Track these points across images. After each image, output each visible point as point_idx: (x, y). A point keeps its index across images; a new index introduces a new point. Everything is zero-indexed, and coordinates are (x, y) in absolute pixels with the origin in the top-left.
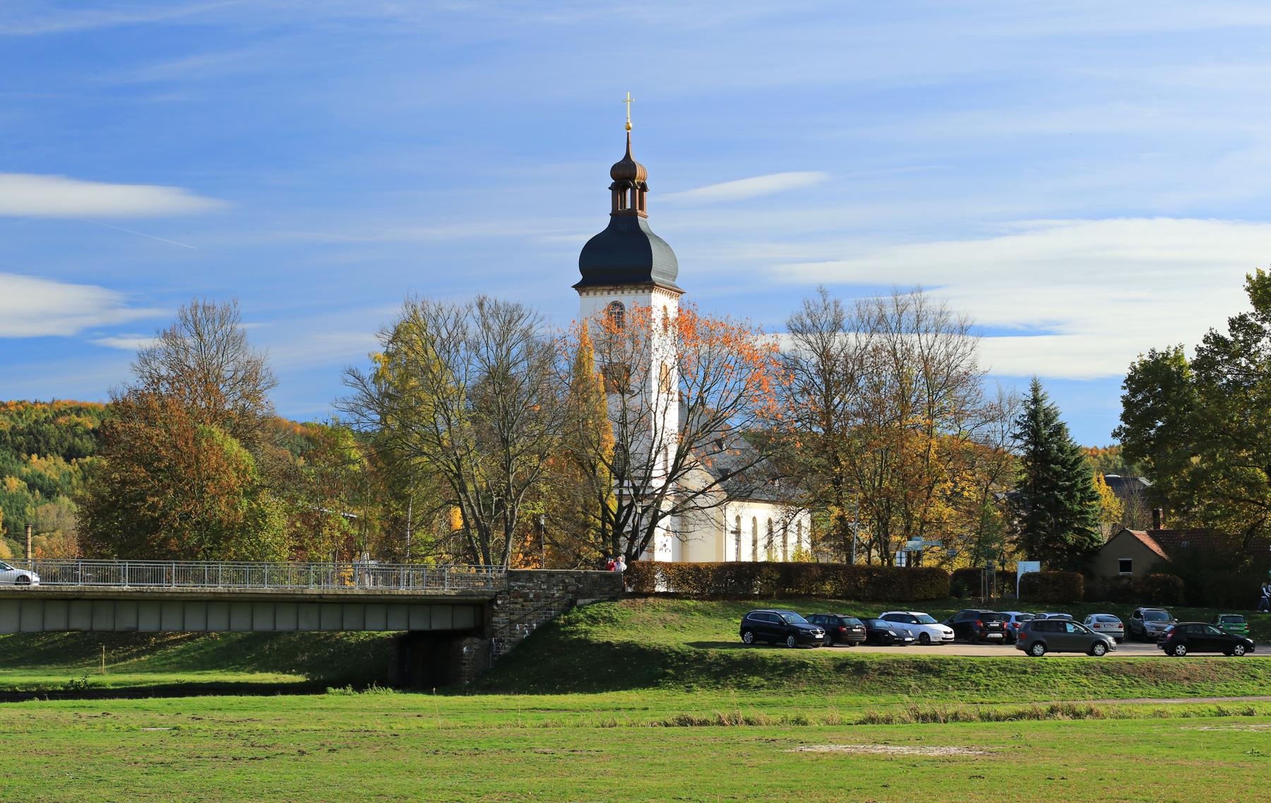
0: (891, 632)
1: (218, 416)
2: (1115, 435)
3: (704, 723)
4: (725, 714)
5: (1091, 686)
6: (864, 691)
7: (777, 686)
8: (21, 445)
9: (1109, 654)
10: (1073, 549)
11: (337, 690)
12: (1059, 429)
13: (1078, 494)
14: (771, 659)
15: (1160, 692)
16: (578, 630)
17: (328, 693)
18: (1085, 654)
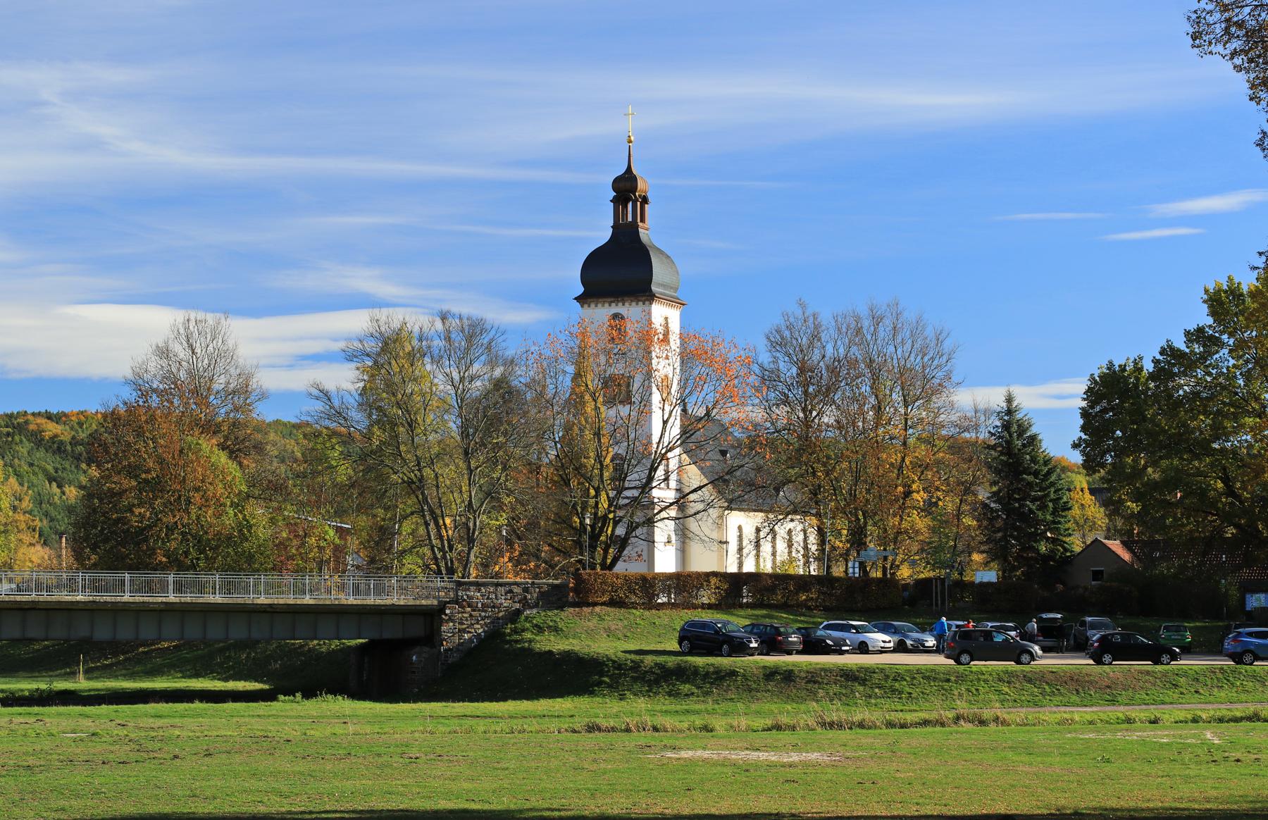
0: (828, 642)
1: (211, 428)
2: (1075, 446)
3: (613, 729)
4: (632, 722)
6: (789, 699)
7: (707, 694)
8: (80, 455)
9: (1036, 662)
10: (1046, 558)
11: (287, 698)
12: (1033, 438)
13: (1051, 505)
14: (703, 668)
17: (278, 701)
18: (1013, 663)
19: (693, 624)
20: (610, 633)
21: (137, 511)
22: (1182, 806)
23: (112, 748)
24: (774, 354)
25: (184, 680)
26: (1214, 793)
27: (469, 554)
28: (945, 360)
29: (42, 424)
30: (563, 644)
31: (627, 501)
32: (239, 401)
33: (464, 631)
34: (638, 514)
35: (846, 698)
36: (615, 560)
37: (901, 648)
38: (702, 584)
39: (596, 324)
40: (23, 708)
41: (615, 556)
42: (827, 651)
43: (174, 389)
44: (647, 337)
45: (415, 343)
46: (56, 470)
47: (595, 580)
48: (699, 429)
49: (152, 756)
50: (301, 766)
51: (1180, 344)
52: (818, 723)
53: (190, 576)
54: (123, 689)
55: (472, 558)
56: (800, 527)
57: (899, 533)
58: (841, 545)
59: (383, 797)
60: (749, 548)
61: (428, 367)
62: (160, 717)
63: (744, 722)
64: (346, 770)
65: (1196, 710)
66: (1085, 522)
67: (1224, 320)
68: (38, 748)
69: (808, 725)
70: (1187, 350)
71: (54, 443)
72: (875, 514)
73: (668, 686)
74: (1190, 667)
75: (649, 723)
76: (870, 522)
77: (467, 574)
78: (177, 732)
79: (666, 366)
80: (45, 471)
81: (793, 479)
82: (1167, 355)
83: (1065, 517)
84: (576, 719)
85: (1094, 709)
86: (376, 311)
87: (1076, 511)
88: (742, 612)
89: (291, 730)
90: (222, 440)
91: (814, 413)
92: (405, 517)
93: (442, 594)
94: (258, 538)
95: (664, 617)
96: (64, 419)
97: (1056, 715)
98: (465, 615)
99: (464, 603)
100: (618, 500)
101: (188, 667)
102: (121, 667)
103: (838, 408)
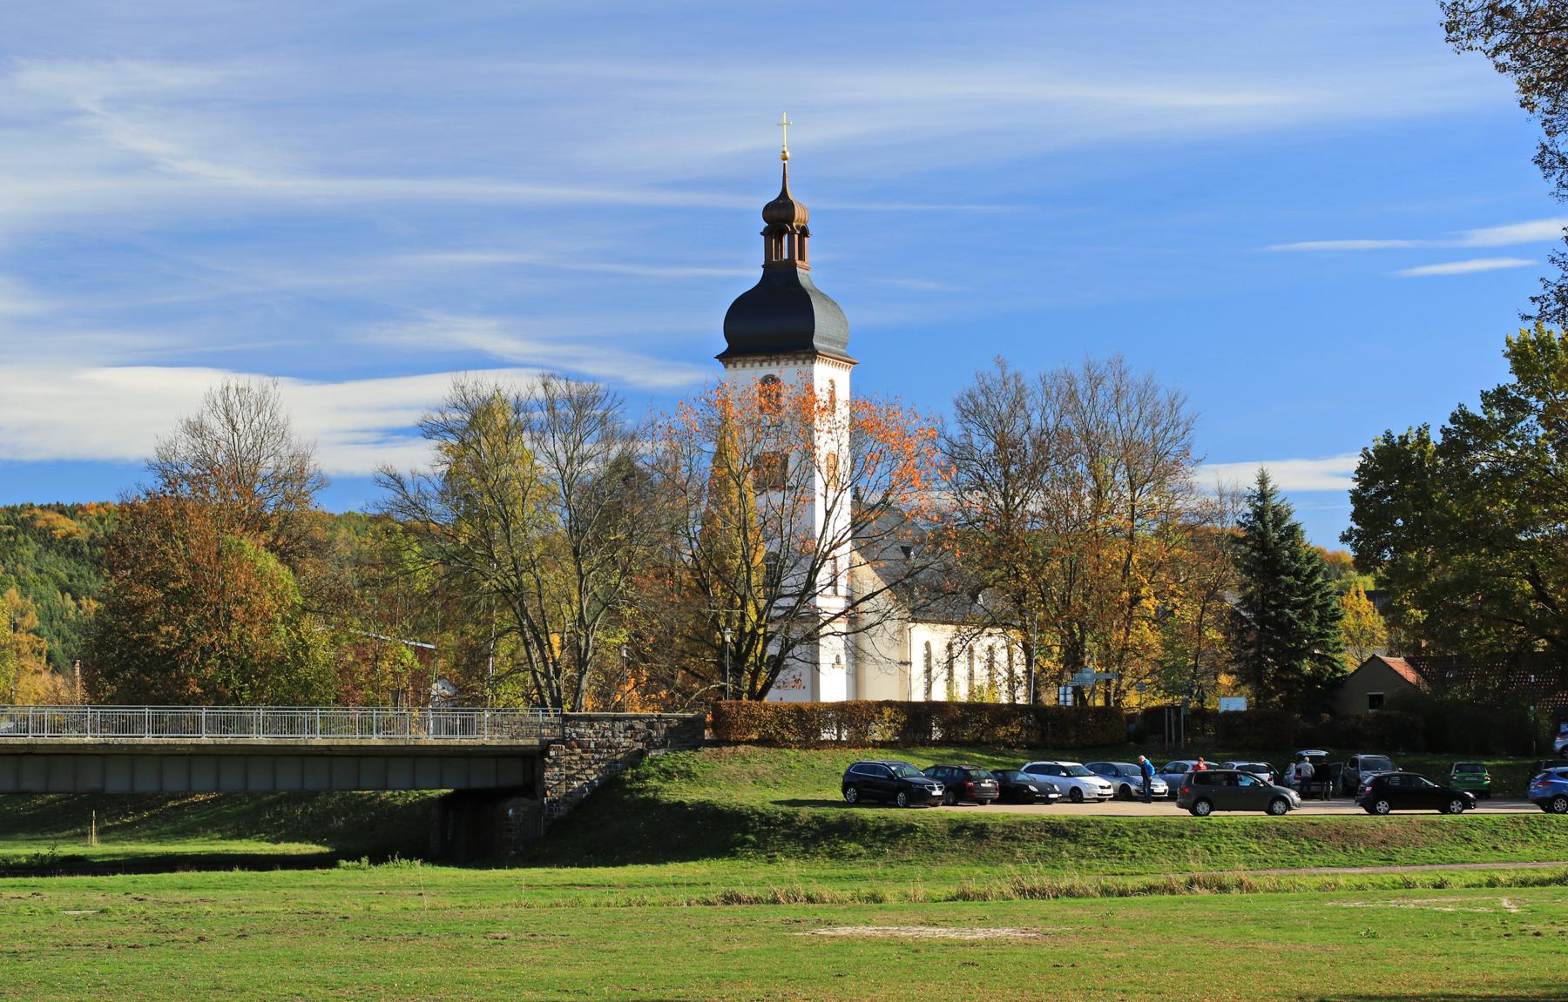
1: (256, 523)
3: (757, 900)
4: (780, 890)
5: (1262, 852)
6: (982, 860)
7: (879, 854)
10: (1315, 677)
11: (350, 863)
12: (1293, 529)
13: (1316, 613)
15: (1347, 859)
16: (647, 787)
17: (339, 867)
18: (1264, 813)
19: (861, 767)
20: (756, 778)
21: (164, 629)
22: (1457, 992)
23: (123, 928)
24: (966, 425)
25: (223, 842)
26: (1500, 975)
27: (580, 680)
28: (1181, 432)
29: (52, 520)
30: (698, 793)
31: (781, 612)
32: (292, 490)
33: (573, 777)
34: (796, 628)
35: (1052, 860)
36: (767, 687)
37: (1123, 795)
38: (873, 717)
39: (740, 389)
40: (18, 879)
41: (766, 682)
42: (1029, 799)
43: (209, 475)
44: (806, 407)
45: (510, 415)
46: (71, 578)
47: (738, 712)
48: (872, 520)
49: (171, 938)
50: (358, 949)
51: (1476, 409)
52: (1015, 890)
53: (232, 710)
54: (145, 854)
55: (584, 684)
56: (1003, 642)
57: (1125, 649)
58: (1052, 666)
59: (454, 987)
60: (940, 673)
61: (528, 445)
62: (190, 888)
63: (921, 890)
64: (413, 954)
65: (1492, 870)
66: (1362, 634)
67: (1531, 378)
68: (29, 929)
69: (1002, 893)
70: (1485, 417)
71: (67, 543)
72: (1095, 626)
73: (829, 845)
74: (1487, 816)
75: (803, 893)
76: (1089, 636)
77: (577, 706)
78: (208, 908)
79: (831, 442)
80: (56, 579)
81: (991, 583)
82: (1460, 423)
83: (1335, 628)
84: (712, 888)
85: (1365, 870)
86: (461, 374)
87: (1349, 620)
88: (924, 752)
89: (352, 905)
90: (271, 539)
91: (1017, 500)
92: (500, 635)
93: (546, 731)
94: (316, 662)
95: (824, 759)
96: (80, 513)
97: (1315, 879)
98: (574, 758)
99: (573, 743)
100: (770, 610)
101: (230, 826)
102: (145, 826)
103: (1047, 493)
